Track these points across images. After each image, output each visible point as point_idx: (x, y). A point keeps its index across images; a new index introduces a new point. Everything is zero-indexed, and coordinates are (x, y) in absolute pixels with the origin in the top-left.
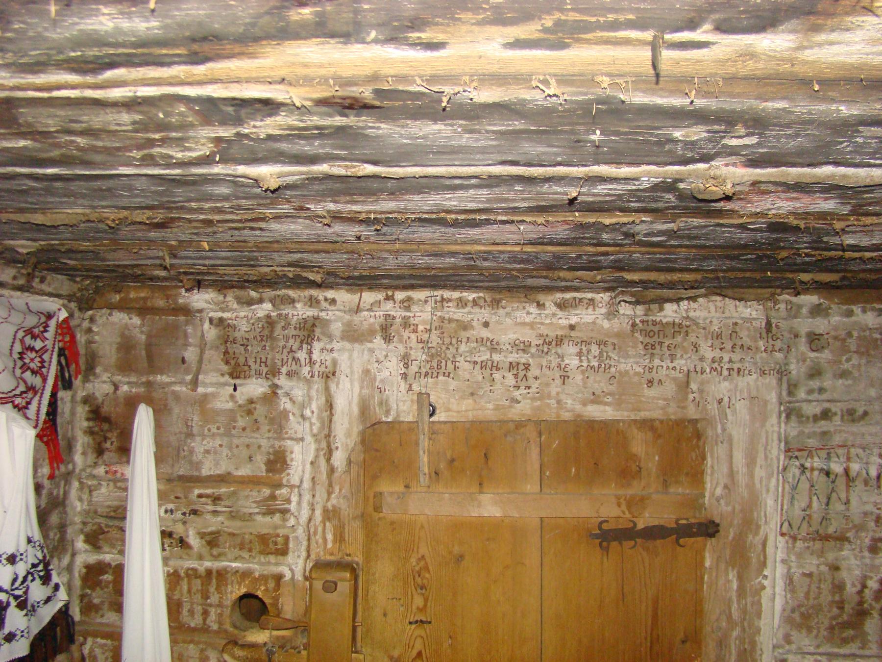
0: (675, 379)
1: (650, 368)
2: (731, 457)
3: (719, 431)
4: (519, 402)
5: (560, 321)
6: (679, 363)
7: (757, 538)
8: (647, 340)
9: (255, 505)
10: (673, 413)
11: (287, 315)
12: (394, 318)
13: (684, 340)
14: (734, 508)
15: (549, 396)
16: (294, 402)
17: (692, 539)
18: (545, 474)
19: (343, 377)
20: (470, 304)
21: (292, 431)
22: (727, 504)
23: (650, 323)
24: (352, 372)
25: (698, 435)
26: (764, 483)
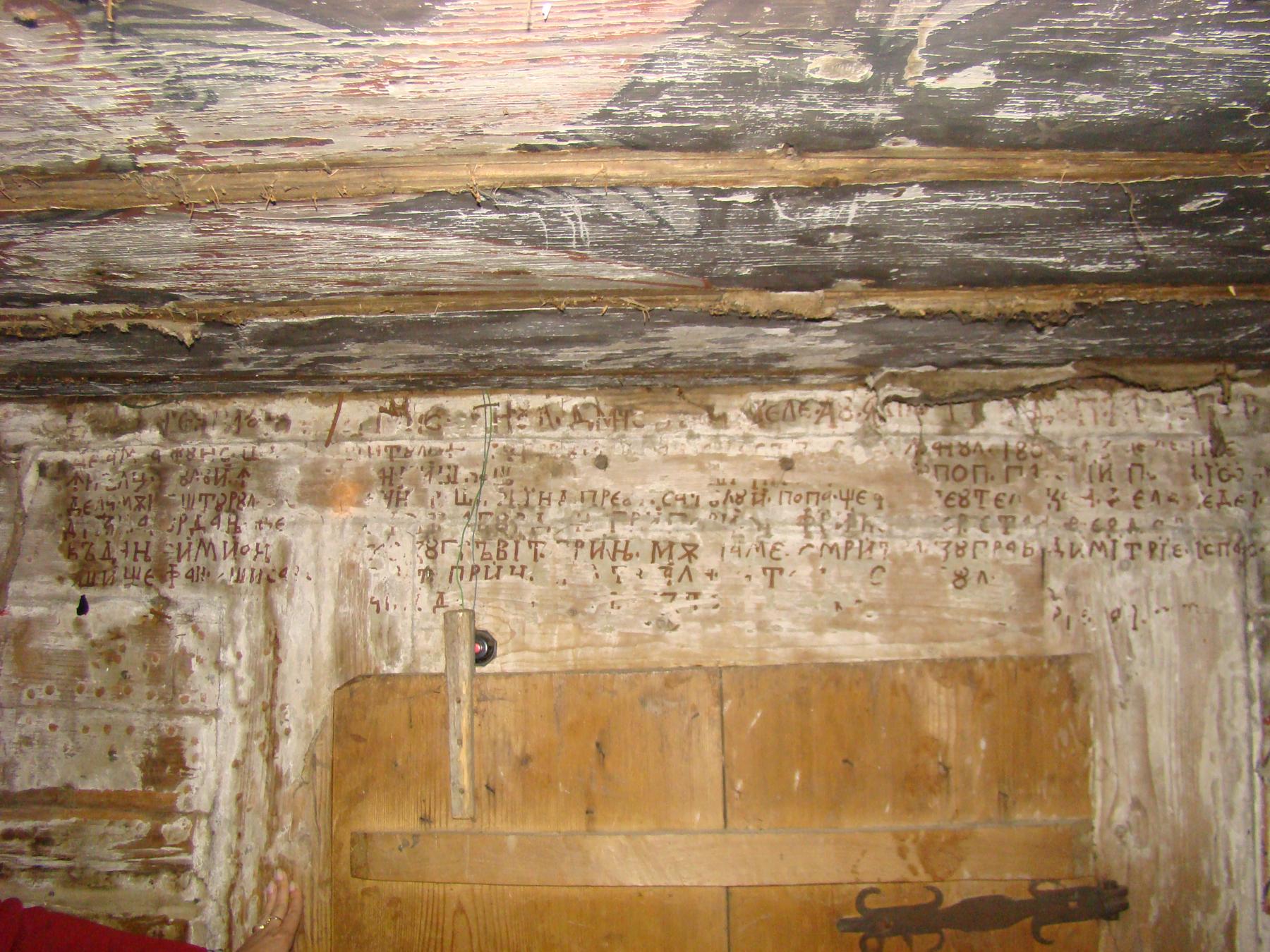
0: (1014, 570)
1: (958, 548)
2: (1144, 737)
3: (1116, 680)
4: (675, 628)
5: (761, 451)
6: (1021, 534)
7: (1213, 919)
8: (951, 487)
9: (118, 855)
10: (1013, 641)
11: (191, 453)
12: (408, 453)
13: (1031, 484)
14: (1156, 852)
15: (740, 613)
16: (201, 635)
17: (1070, 927)
18: (733, 787)
19: (301, 579)
20: (567, 420)
21: (197, 697)
22: (1142, 843)
23: (955, 451)
24: (319, 569)
25: (1073, 690)
26: (1220, 794)
